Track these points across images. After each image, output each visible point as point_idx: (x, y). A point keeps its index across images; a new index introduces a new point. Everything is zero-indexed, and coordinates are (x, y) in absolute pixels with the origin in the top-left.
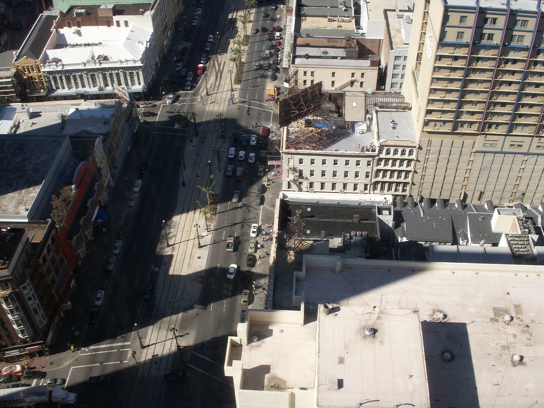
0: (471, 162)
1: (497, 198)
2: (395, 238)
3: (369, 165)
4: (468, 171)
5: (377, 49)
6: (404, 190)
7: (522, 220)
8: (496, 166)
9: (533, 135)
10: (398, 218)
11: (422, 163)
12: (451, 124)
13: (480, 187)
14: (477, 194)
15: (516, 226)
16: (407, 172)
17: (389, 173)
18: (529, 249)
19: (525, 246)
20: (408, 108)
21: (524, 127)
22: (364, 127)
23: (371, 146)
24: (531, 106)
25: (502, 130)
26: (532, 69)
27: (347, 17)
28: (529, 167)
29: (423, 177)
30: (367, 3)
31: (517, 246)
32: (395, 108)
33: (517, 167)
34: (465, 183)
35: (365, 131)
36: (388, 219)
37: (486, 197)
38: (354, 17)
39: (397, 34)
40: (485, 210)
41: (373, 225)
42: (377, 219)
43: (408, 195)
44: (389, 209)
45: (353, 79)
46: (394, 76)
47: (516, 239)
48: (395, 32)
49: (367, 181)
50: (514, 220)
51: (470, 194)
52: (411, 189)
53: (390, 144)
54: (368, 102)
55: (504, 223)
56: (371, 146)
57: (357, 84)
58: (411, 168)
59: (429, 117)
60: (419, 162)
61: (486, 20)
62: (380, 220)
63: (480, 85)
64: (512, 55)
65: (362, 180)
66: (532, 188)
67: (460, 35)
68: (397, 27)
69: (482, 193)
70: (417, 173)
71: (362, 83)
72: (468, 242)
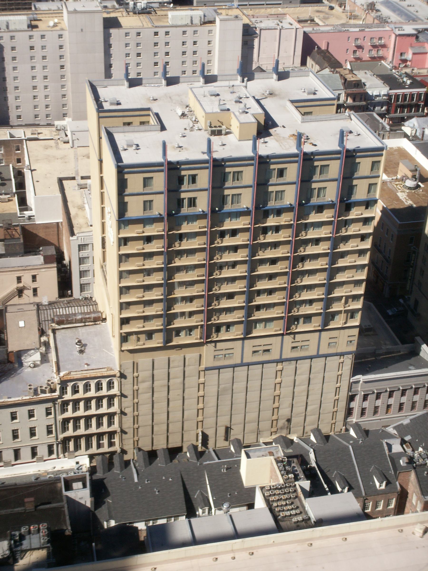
0: (201, 386)
1: (252, 432)
2: (97, 523)
3: (50, 414)
4: (201, 399)
5: (56, 237)
6: (111, 444)
7: (282, 461)
8: (240, 386)
9: (282, 332)
10: (99, 490)
11: (130, 397)
12: (242, 326)
13: (224, 421)
14: (221, 431)
15: (275, 472)
16: (111, 416)
17: (82, 422)
18: (299, 504)
19: (290, 501)
20: (100, 319)
21: (268, 324)
22: (36, 357)
23: (49, 385)
24: (270, 292)
25: (237, 332)
26: (262, 240)
27: (6, 194)
28: (287, 379)
29: (136, 419)
30: (32, 171)
31: (279, 503)
32: (81, 321)
33: (269, 382)
34: (200, 418)
35: (39, 363)
36: (82, 495)
37: (236, 433)
38: (16, 193)
39: (80, 213)
40: (231, 455)
41: (58, 512)
42: (65, 499)
43: (119, 450)
44: (82, 479)
45: (21, 285)
46: (82, 274)
47: (277, 492)
48: (76, 209)
49: (51, 439)
50: (272, 463)
51: (210, 433)
52: (121, 440)
53: (76, 377)
54: (42, 318)
55: (258, 471)
56: (49, 385)
57: (28, 293)
58: (115, 408)
59: (127, 329)
60: (126, 397)
61: (181, 180)
62: (70, 501)
63: (190, 273)
64: (229, 225)
65: (42, 439)
66: (299, 409)
67: (148, 205)
68: (79, 201)
69: (228, 430)
70: (125, 414)
71: (35, 290)
72: (210, 509)
